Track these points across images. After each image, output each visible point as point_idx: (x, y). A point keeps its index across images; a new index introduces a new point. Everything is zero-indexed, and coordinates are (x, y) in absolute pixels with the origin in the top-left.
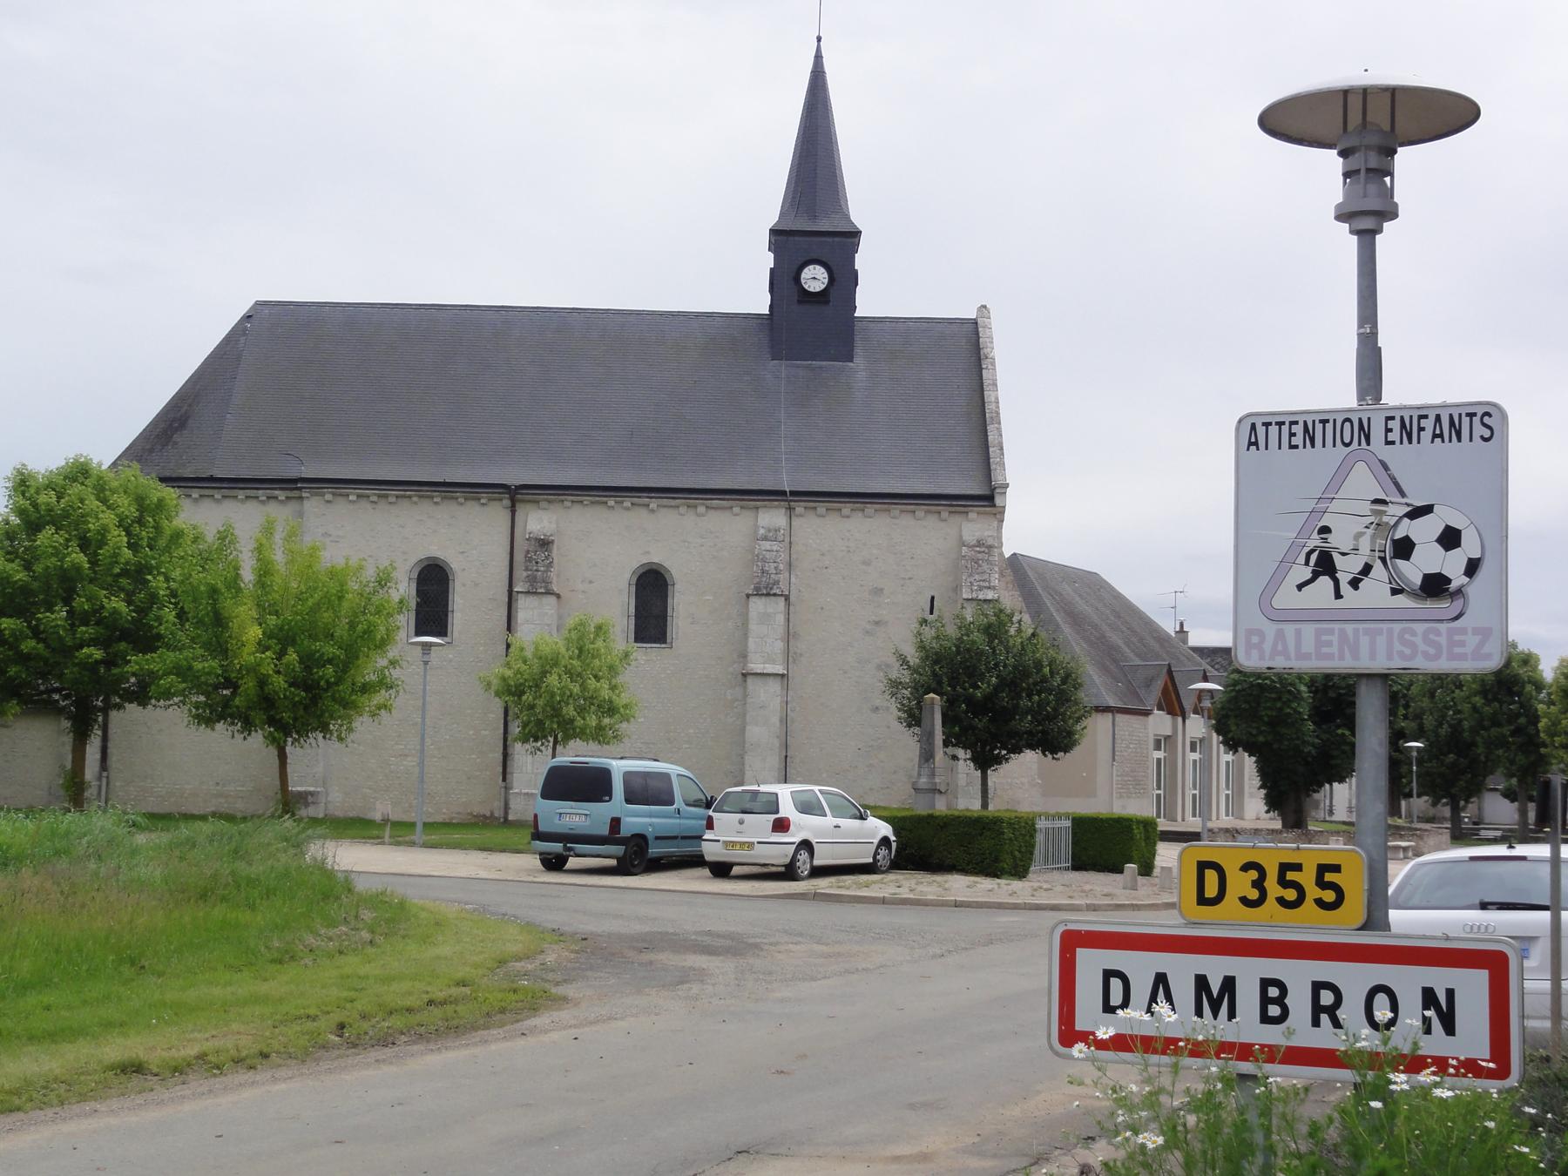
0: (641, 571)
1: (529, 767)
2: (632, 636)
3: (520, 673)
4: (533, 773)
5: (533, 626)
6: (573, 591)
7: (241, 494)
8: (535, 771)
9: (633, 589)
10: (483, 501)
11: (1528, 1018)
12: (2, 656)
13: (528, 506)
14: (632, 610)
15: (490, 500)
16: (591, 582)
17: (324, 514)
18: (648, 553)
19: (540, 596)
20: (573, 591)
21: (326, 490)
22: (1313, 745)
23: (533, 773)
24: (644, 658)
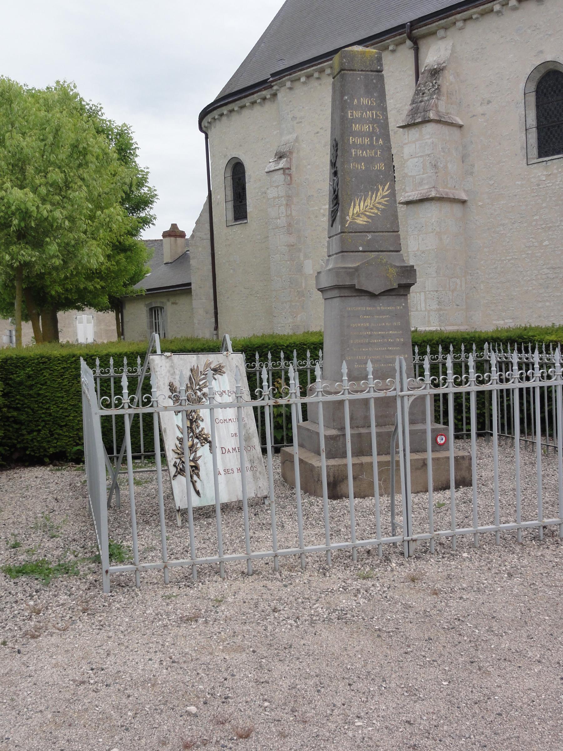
0: (538, 76)
1: (423, 305)
2: (534, 151)
3: (12, 172)
4: (425, 311)
5: (416, 160)
6: (474, 116)
7: (247, 101)
8: (428, 308)
9: (532, 99)
10: (391, 48)
11: (154, 311)
12: (2, 214)
13: (430, 40)
14: (532, 120)
15: (397, 45)
16: (489, 102)
17: (290, 101)
18: (541, 52)
19: (420, 126)
20: (474, 116)
21: (284, 79)
22: (359, 107)
23: (425, 311)
24: (545, 173)
